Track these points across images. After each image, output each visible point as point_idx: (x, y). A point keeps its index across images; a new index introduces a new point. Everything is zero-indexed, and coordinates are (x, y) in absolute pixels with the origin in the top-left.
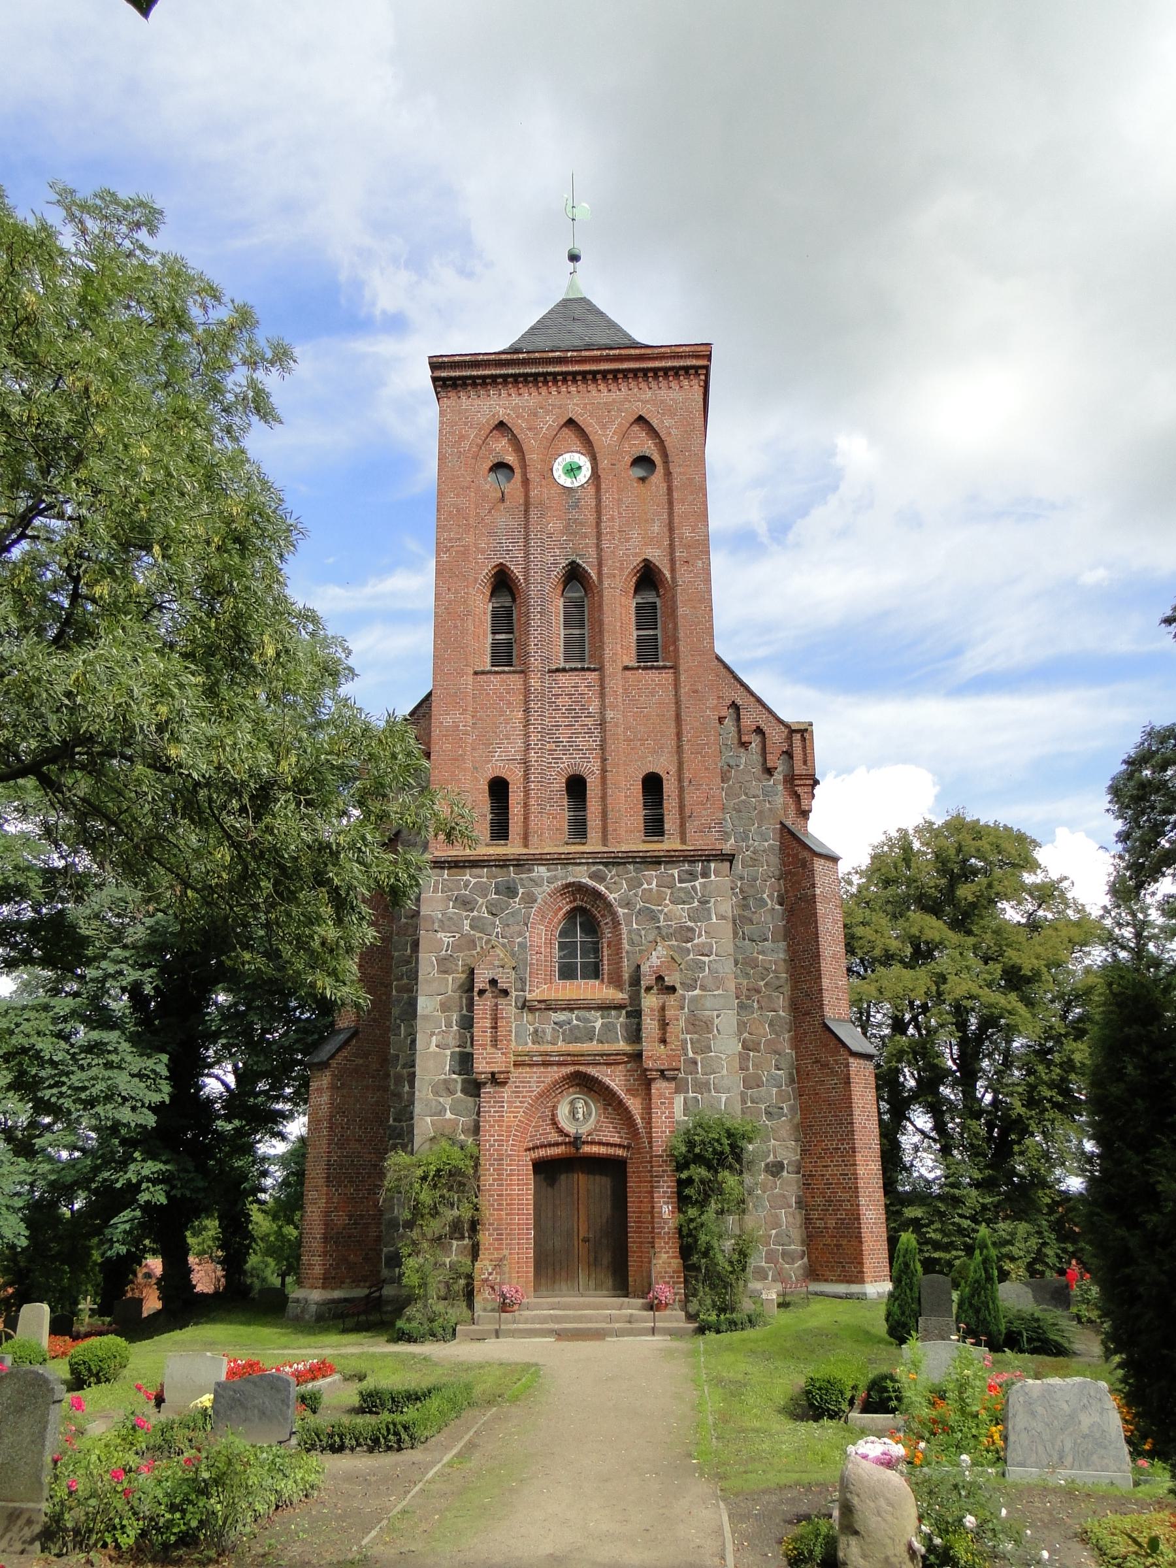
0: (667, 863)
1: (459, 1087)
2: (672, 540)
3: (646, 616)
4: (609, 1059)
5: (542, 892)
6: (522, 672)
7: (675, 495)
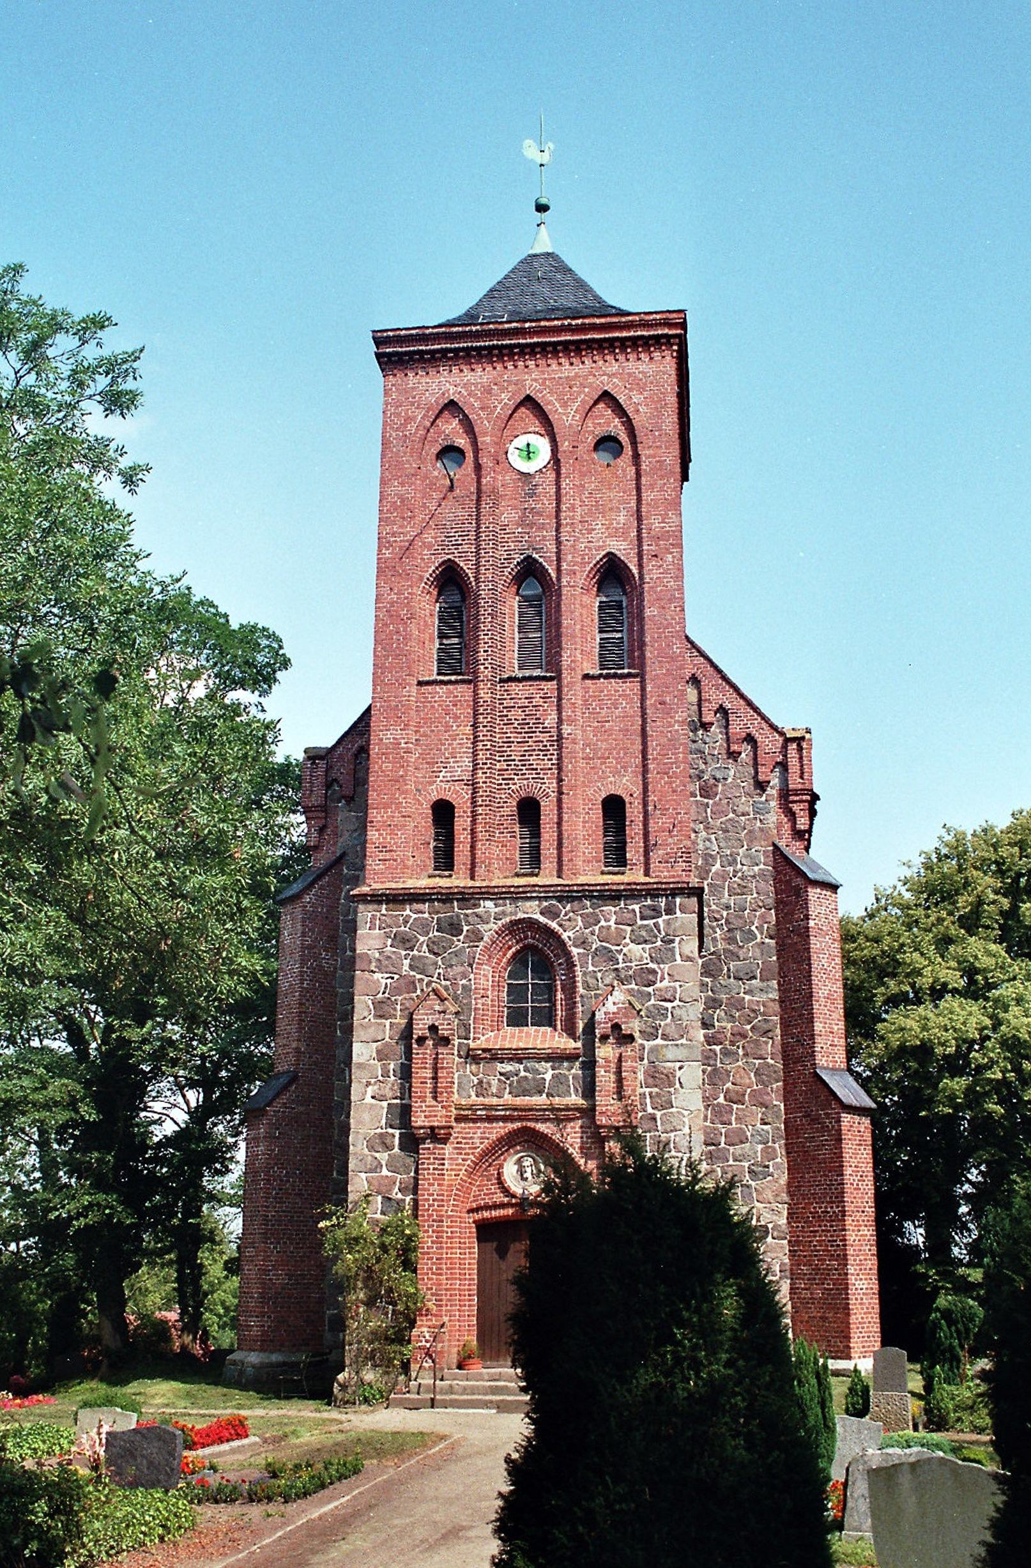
0: (627, 898)
1: (397, 1141)
2: (639, 531)
3: (610, 616)
4: (560, 1116)
5: (489, 930)
6: (469, 682)
7: (643, 480)
